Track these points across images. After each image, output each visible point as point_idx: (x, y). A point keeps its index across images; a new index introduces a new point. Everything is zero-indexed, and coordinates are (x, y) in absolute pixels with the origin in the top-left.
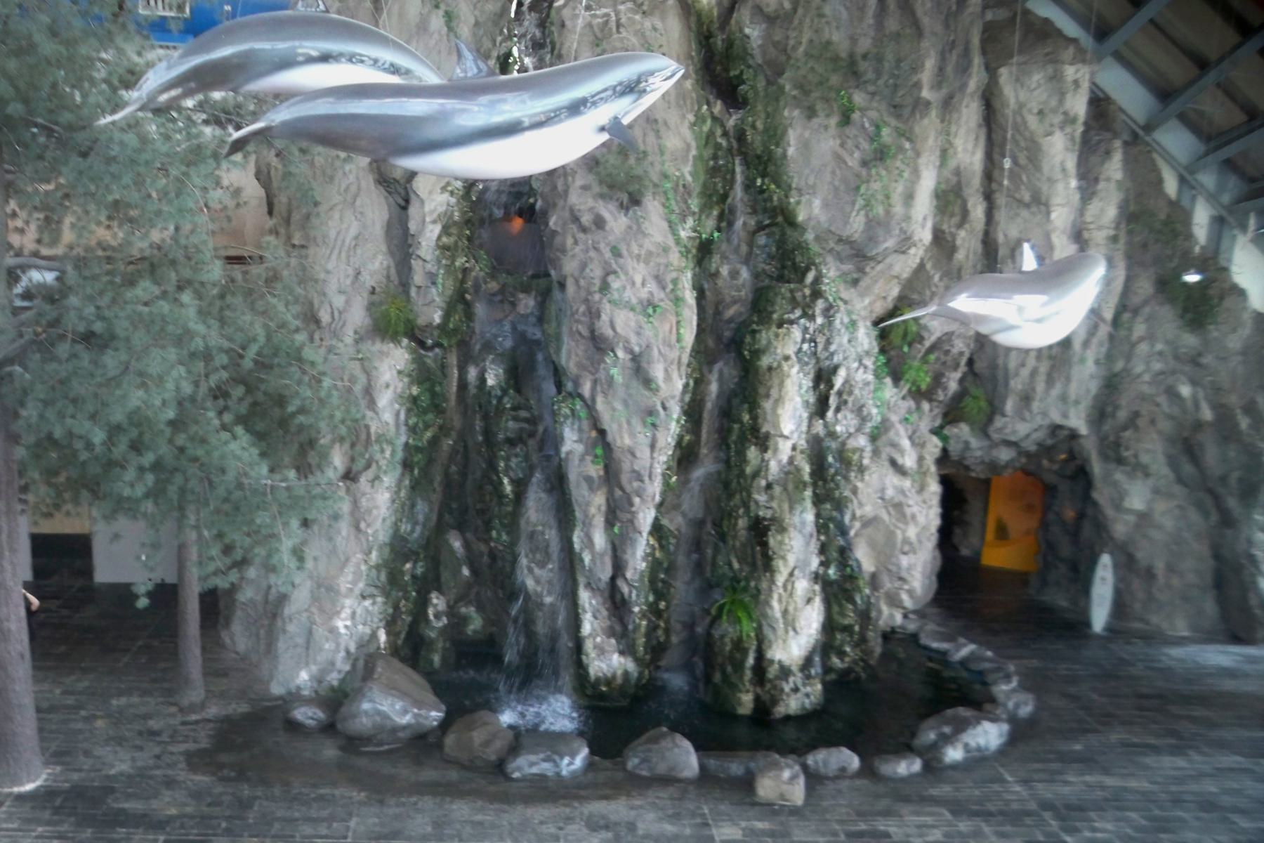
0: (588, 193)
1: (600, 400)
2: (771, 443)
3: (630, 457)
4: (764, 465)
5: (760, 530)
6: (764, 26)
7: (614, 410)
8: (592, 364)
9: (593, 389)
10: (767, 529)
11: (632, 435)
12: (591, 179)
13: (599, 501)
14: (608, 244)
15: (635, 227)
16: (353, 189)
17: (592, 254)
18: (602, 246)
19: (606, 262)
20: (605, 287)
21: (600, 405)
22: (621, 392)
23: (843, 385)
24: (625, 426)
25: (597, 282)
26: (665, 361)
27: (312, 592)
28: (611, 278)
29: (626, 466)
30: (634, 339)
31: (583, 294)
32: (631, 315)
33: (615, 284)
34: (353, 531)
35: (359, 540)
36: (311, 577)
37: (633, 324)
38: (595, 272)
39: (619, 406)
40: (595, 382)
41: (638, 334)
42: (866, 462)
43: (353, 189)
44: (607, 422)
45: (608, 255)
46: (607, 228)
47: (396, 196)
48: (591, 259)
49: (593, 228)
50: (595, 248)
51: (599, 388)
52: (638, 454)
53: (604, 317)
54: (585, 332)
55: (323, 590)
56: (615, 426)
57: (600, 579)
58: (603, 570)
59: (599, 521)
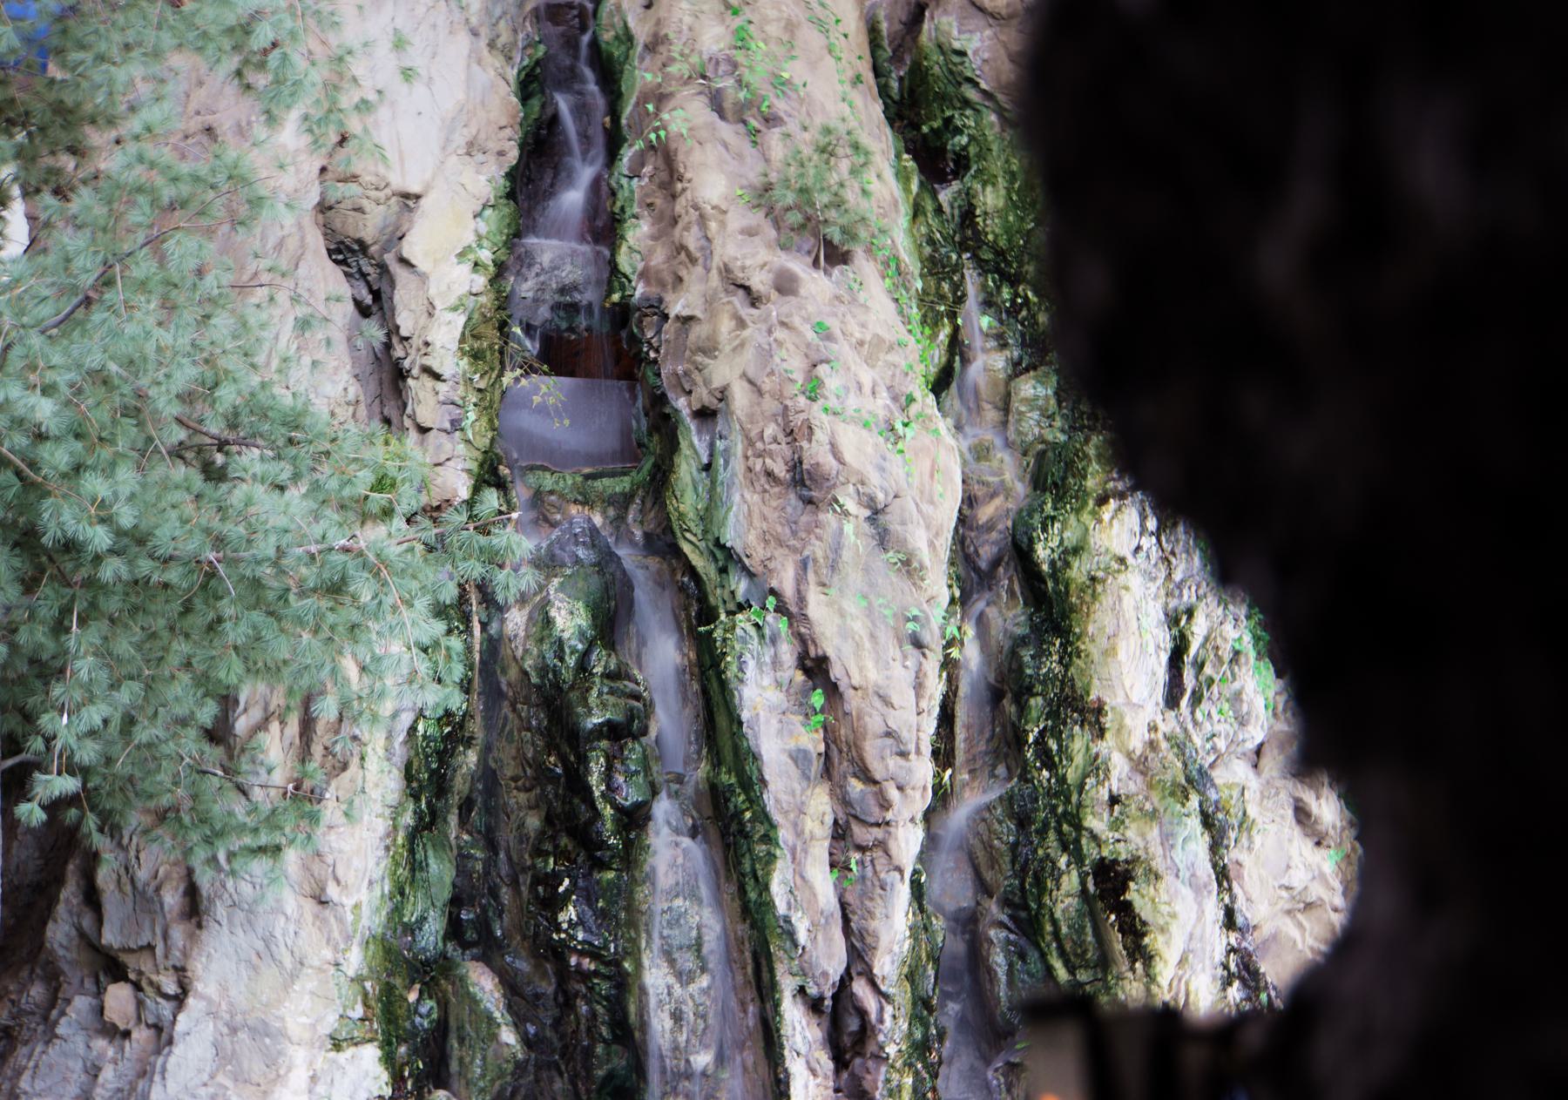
0: (757, 239)
1: (814, 597)
2: (1108, 721)
3: (878, 703)
4: (1096, 767)
5: (1112, 882)
6: (988, 32)
7: (842, 614)
8: (794, 533)
9: (800, 580)
10: (1127, 877)
11: (882, 663)
12: (757, 218)
13: (820, 806)
14: (806, 320)
15: (846, 298)
16: (292, 244)
17: (780, 334)
18: (796, 321)
19: (808, 345)
20: (813, 390)
21: (817, 607)
22: (854, 578)
23: (1203, 645)
24: (867, 645)
25: (799, 377)
26: (928, 527)
27: (216, 1046)
28: (822, 370)
29: (874, 724)
30: (874, 479)
31: (770, 405)
32: (864, 433)
33: (833, 382)
34: (310, 906)
35: (325, 921)
36: (213, 1014)
37: (870, 450)
38: (795, 365)
39: (852, 606)
40: (804, 565)
41: (882, 469)
42: (1252, 812)
43: (292, 244)
44: (830, 643)
45: (810, 336)
46: (802, 292)
47: (361, 285)
48: (780, 344)
49: (774, 295)
50: (783, 324)
51: (811, 576)
52: (895, 700)
53: (819, 435)
54: (780, 470)
55: (243, 1035)
56: (848, 649)
57: (825, 974)
58: (830, 957)
59: (820, 851)
